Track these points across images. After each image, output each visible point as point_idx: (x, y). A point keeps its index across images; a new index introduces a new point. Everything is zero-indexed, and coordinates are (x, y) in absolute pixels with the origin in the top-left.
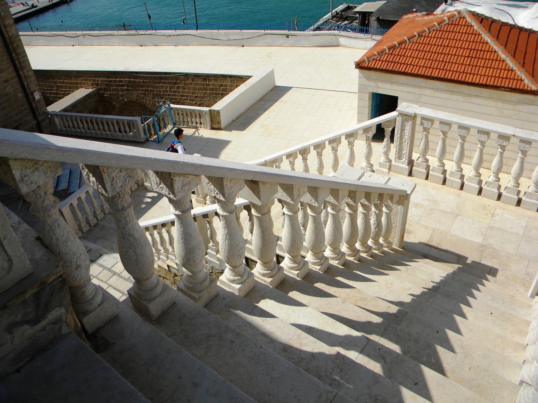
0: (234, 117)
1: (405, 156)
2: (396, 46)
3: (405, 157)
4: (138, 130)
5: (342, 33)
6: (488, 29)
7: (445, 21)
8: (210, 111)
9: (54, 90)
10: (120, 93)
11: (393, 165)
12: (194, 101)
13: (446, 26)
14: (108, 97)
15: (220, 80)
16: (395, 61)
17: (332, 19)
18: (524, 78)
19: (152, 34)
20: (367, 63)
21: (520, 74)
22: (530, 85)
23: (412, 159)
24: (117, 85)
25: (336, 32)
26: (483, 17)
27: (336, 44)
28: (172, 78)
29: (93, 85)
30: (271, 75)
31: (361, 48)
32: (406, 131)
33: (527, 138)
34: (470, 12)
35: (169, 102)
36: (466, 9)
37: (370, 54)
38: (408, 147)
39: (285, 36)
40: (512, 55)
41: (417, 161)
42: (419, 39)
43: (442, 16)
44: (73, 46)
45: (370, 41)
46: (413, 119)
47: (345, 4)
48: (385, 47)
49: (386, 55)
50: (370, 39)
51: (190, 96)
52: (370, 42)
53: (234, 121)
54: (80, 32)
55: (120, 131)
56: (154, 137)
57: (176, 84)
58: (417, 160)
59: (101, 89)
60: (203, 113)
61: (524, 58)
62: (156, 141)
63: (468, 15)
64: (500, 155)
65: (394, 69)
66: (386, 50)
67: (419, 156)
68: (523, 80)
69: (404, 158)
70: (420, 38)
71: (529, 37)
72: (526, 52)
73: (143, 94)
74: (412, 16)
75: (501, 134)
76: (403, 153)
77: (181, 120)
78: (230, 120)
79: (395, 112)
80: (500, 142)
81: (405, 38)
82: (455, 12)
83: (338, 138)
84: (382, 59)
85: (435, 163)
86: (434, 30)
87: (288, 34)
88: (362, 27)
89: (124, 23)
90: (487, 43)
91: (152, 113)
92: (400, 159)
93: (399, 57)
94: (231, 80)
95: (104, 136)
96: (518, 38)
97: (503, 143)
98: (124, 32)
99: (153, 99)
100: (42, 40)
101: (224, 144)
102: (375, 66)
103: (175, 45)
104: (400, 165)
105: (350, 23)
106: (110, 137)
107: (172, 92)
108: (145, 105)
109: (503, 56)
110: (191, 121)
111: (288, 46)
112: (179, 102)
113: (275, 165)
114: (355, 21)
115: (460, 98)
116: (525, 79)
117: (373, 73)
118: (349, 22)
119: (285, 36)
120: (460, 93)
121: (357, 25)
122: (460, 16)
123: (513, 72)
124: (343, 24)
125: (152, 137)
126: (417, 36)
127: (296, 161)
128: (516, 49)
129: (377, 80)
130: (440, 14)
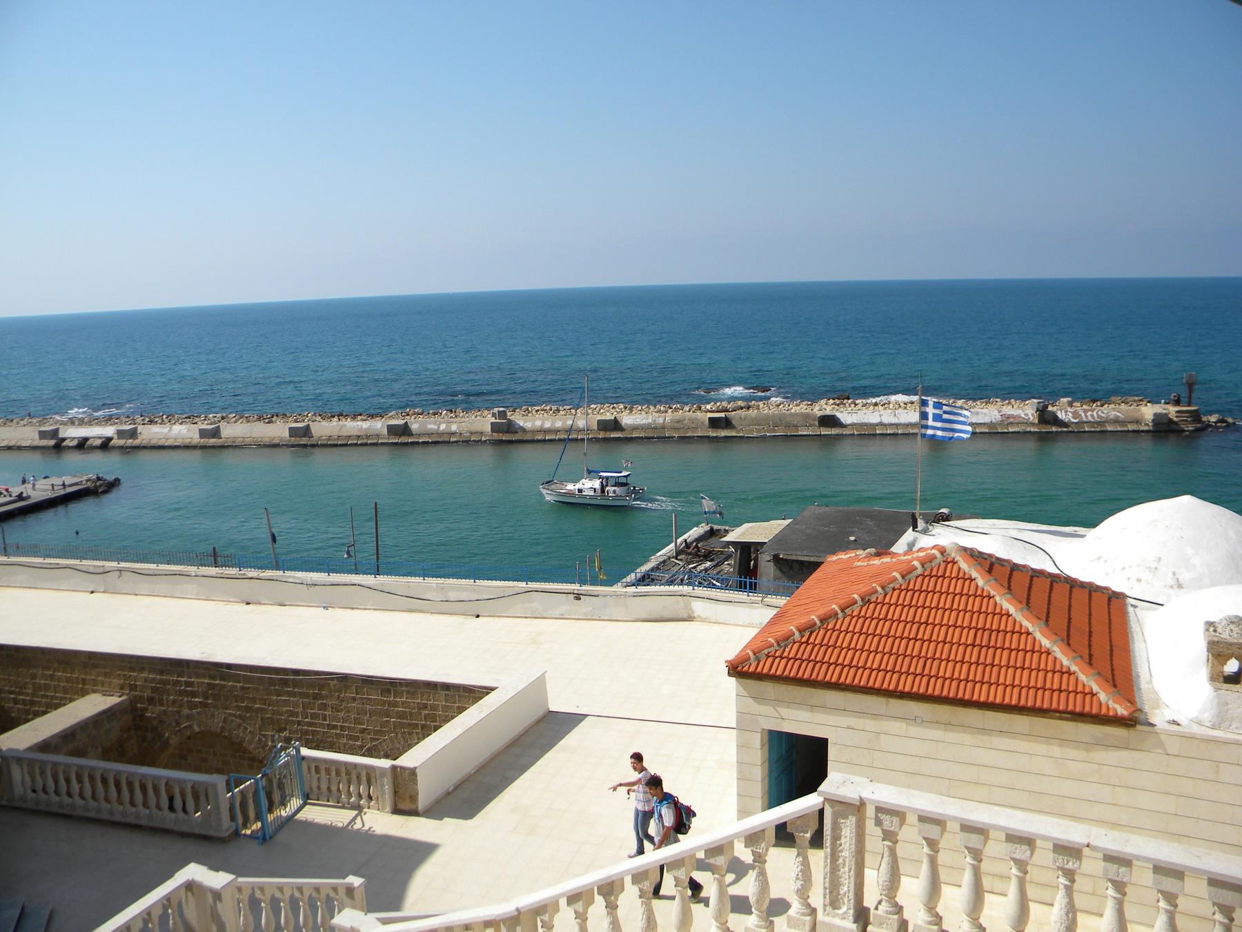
0: (449, 784)
1: (846, 900)
2: (816, 624)
3: (846, 902)
4: (217, 807)
5: (700, 591)
6: (1006, 584)
7: (916, 569)
8: (394, 768)
9: (27, 694)
10: (186, 711)
11: (820, 921)
12: (358, 740)
13: (920, 579)
14: (155, 718)
15: (422, 694)
16: (816, 657)
17: (677, 559)
18: (1095, 688)
19: (275, 578)
20: (754, 665)
21: (1087, 682)
22: (1111, 703)
23: (865, 905)
24: (181, 693)
25: (686, 589)
26: (993, 560)
27: (685, 616)
28: (311, 685)
29: (122, 688)
30: (539, 686)
31: (740, 623)
32: (843, 840)
33: (1118, 852)
34: (965, 549)
35: (297, 743)
36: (957, 544)
37: (759, 644)
38: (852, 879)
39: (572, 596)
40: (1063, 640)
41: (876, 912)
42: (864, 609)
43: (910, 557)
44: (92, 592)
45: (761, 608)
46: (859, 811)
47: (703, 525)
48: (792, 627)
49: (796, 646)
50: (761, 605)
51: (349, 727)
52: (760, 610)
53: (448, 794)
54: (114, 564)
55: (171, 808)
56: (254, 827)
57: (318, 699)
58: (876, 908)
59: (139, 699)
60: (378, 772)
61: (1090, 646)
62: (257, 838)
63: (960, 556)
64: (1066, 892)
65: (814, 676)
66: (793, 635)
67: (880, 898)
68: (1096, 694)
69: (844, 904)
70: (867, 606)
71: (1090, 600)
72: (1090, 632)
73: (240, 717)
74: (847, 556)
75: (1060, 843)
76: (842, 892)
77: (324, 786)
78: (439, 792)
79: (815, 794)
80: (1061, 860)
81: (834, 606)
82: (934, 551)
83: (689, 856)
84: (786, 654)
85: (919, 914)
86: (894, 589)
87: (580, 592)
88: (741, 577)
89: (214, 548)
90: (1009, 615)
91: (257, 762)
92: (835, 908)
93: (823, 649)
94: (446, 695)
95: (131, 820)
96: (1070, 602)
97: (1068, 863)
98: (213, 571)
99: (260, 730)
100: (22, 575)
101: (421, 851)
102: (773, 671)
103: (324, 607)
104: (837, 921)
105: (715, 566)
106: (144, 822)
107: (307, 718)
108: (240, 744)
109: (1046, 643)
110: (346, 790)
111: (578, 619)
112: (322, 741)
113: (541, 921)
114: (726, 563)
115: (967, 738)
116: (1099, 690)
117: (768, 687)
118: (714, 563)
119: (572, 596)
120: (964, 727)
121: (732, 570)
122: (945, 559)
123: (1072, 677)
124: (702, 567)
125: (248, 825)
126: (860, 603)
127: (591, 910)
128: (1069, 627)
129: (778, 702)
130: (905, 554)
